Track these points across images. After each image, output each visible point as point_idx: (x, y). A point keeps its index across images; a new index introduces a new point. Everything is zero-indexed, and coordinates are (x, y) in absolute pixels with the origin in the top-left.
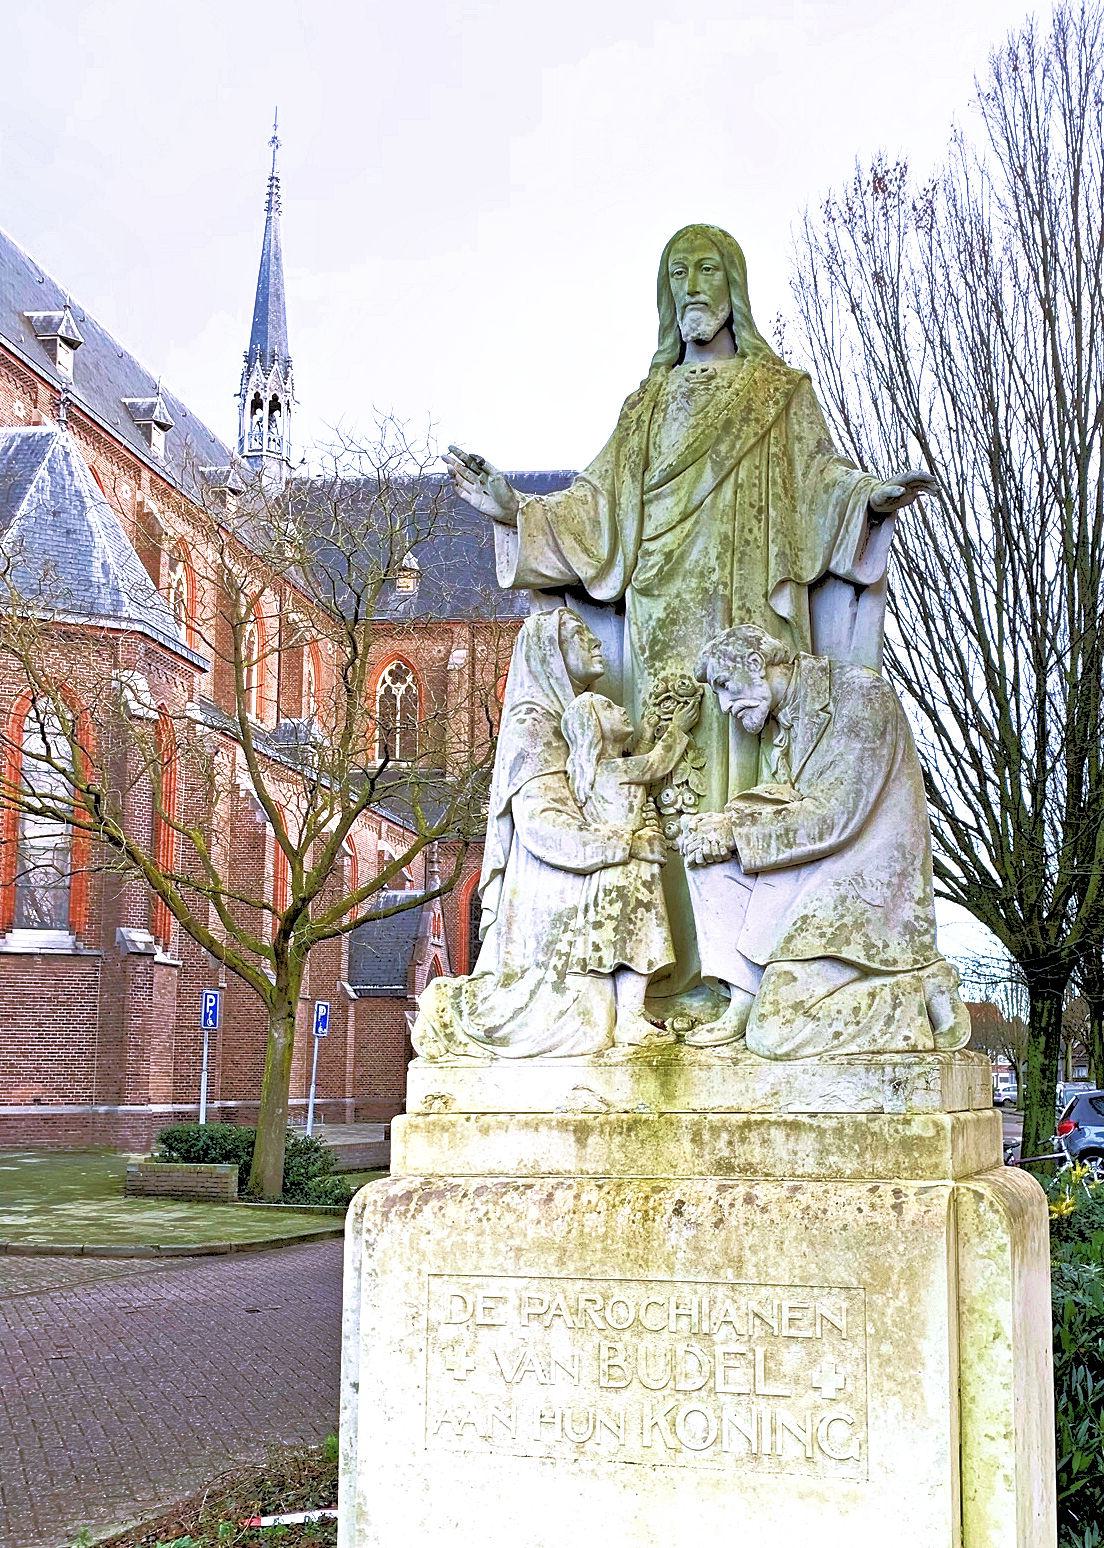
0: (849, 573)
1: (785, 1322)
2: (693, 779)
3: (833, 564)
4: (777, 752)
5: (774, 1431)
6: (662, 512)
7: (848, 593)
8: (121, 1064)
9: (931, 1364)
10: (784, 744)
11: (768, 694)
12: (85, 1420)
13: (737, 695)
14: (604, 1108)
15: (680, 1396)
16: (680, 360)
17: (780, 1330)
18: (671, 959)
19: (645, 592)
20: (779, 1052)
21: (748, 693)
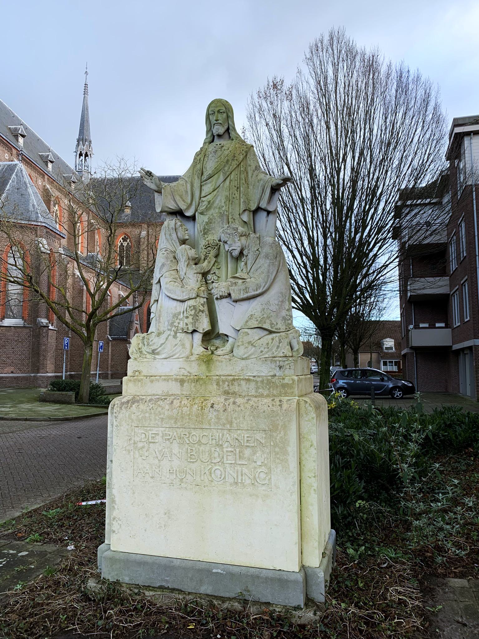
4: (243, 263)
5: (242, 475)
6: (207, 188)
7: (265, 214)
10: (245, 261)
14: (189, 375)
15: (213, 464)
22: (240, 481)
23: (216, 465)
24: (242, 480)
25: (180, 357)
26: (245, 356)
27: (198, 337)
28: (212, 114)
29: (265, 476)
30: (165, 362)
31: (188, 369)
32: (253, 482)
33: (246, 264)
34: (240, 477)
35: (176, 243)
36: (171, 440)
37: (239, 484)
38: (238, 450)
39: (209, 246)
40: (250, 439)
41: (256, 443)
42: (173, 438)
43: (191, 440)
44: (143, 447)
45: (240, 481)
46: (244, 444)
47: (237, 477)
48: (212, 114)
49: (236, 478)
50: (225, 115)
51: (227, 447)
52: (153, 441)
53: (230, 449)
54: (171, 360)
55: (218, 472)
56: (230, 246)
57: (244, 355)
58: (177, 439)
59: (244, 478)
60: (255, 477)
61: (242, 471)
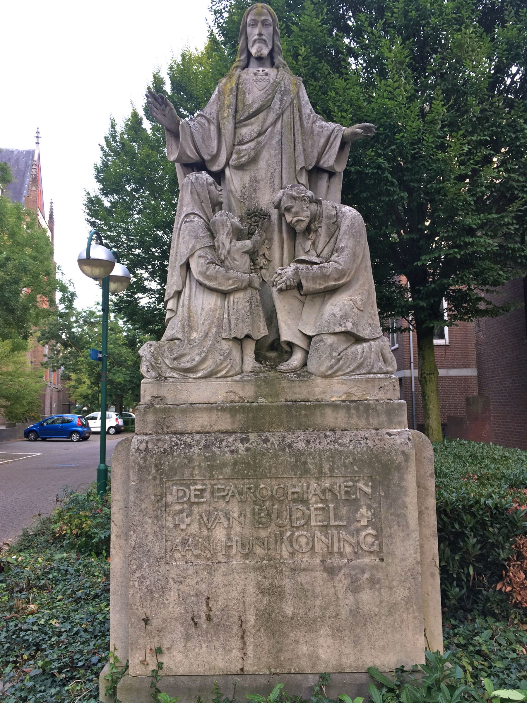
0: (331, 167)
1: (343, 493)
2: (267, 253)
3: (321, 162)
4: (310, 242)
5: (339, 541)
6: (245, 131)
7: (326, 176)
8: (427, 413)
9: (410, 507)
10: (313, 238)
11: (309, 215)
12: (52, 646)
13: (296, 214)
14: (242, 400)
15: (295, 529)
16: (247, 66)
17: (340, 497)
18: (267, 333)
19: (240, 167)
20: (327, 374)
21: (301, 214)
22: (336, 549)
23: (298, 531)
24: (339, 549)
25: (228, 375)
26: (330, 372)
27: (250, 348)
28: (253, 25)
29: (373, 540)
30: (202, 383)
31: (241, 393)
32: (356, 550)
33: (313, 244)
34: (336, 545)
35: (208, 207)
36: (227, 498)
37: (336, 554)
38: (331, 506)
39: (256, 215)
40: (349, 489)
41: (358, 494)
42: (230, 494)
43: (258, 495)
44: (181, 511)
45: (336, 549)
46: (340, 497)
47: (332, 543)
48: (253, 25)
49: (330, 545)
50: (271, 29)
51: (316, 503)
52: (196, 500)
53: (320, 505)
54: (213, 380)
55: (303, 540)
56: (296, 214)
57: (327, 371)
58: (237, 496)
59: (342, 546)
60: (358, 542)
61: (339, 537)
